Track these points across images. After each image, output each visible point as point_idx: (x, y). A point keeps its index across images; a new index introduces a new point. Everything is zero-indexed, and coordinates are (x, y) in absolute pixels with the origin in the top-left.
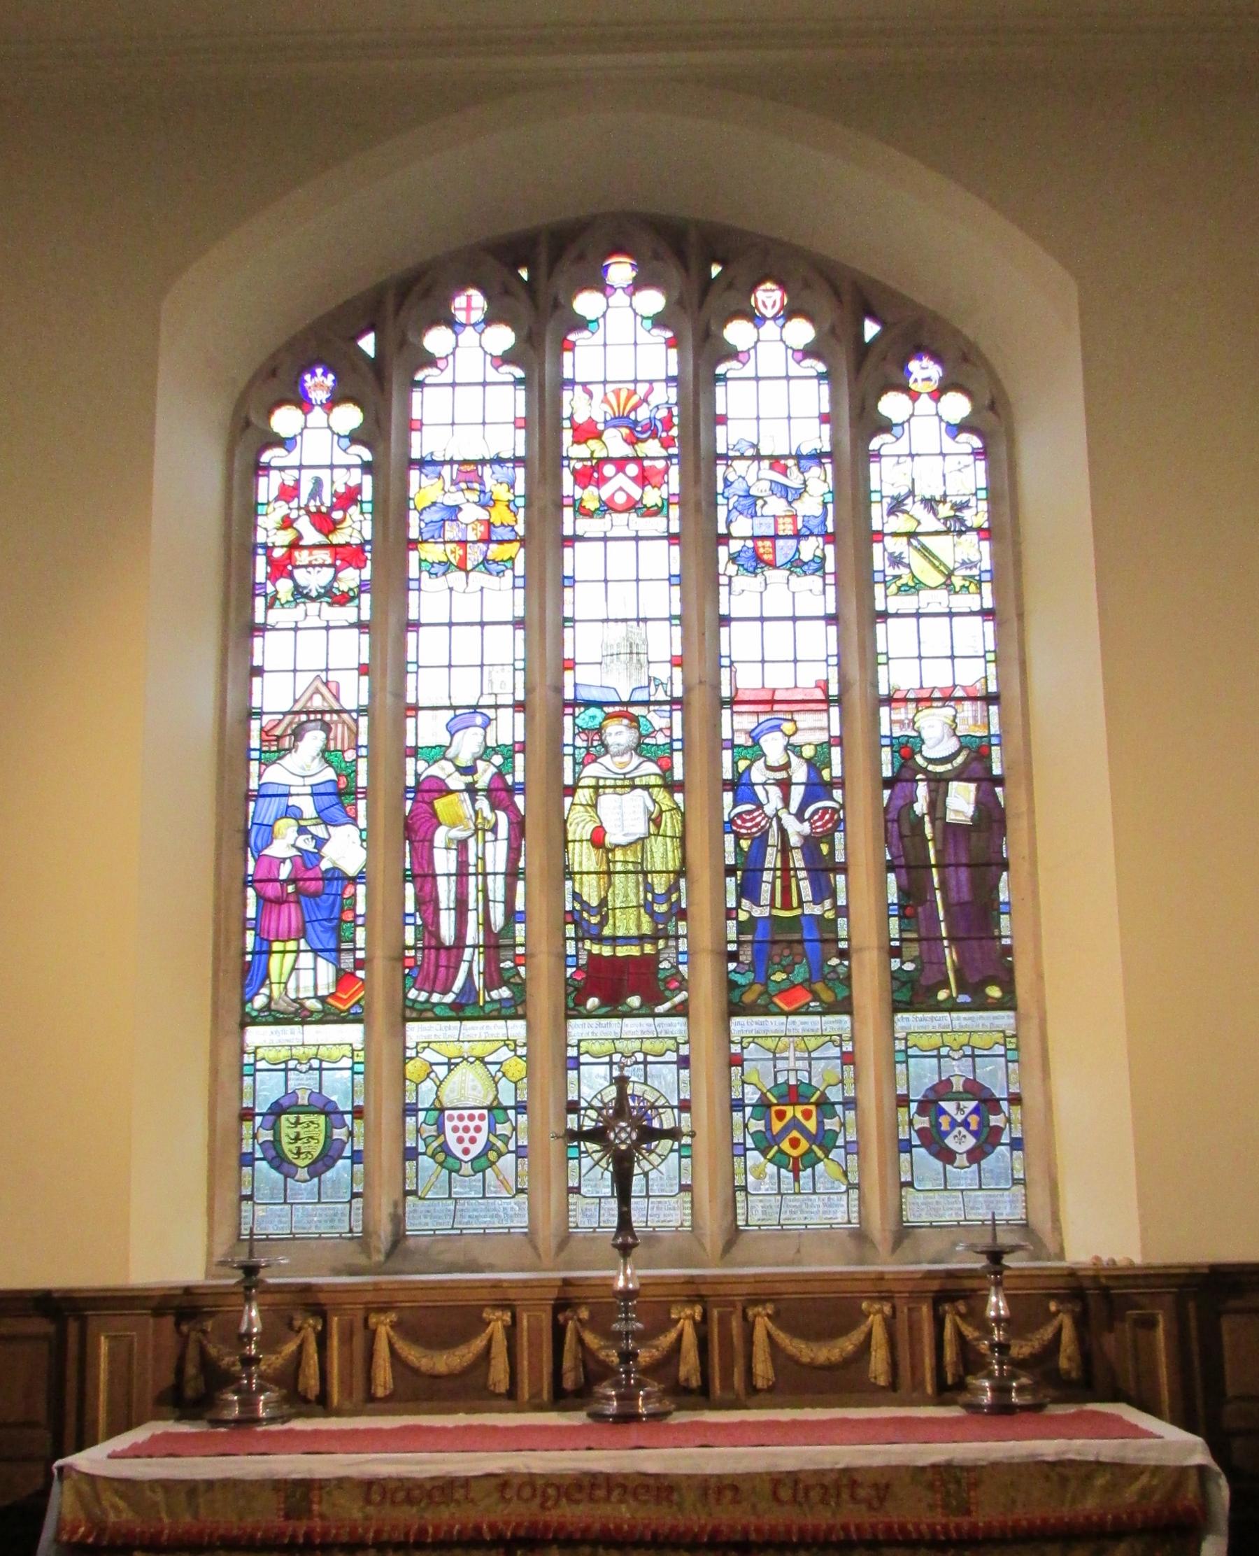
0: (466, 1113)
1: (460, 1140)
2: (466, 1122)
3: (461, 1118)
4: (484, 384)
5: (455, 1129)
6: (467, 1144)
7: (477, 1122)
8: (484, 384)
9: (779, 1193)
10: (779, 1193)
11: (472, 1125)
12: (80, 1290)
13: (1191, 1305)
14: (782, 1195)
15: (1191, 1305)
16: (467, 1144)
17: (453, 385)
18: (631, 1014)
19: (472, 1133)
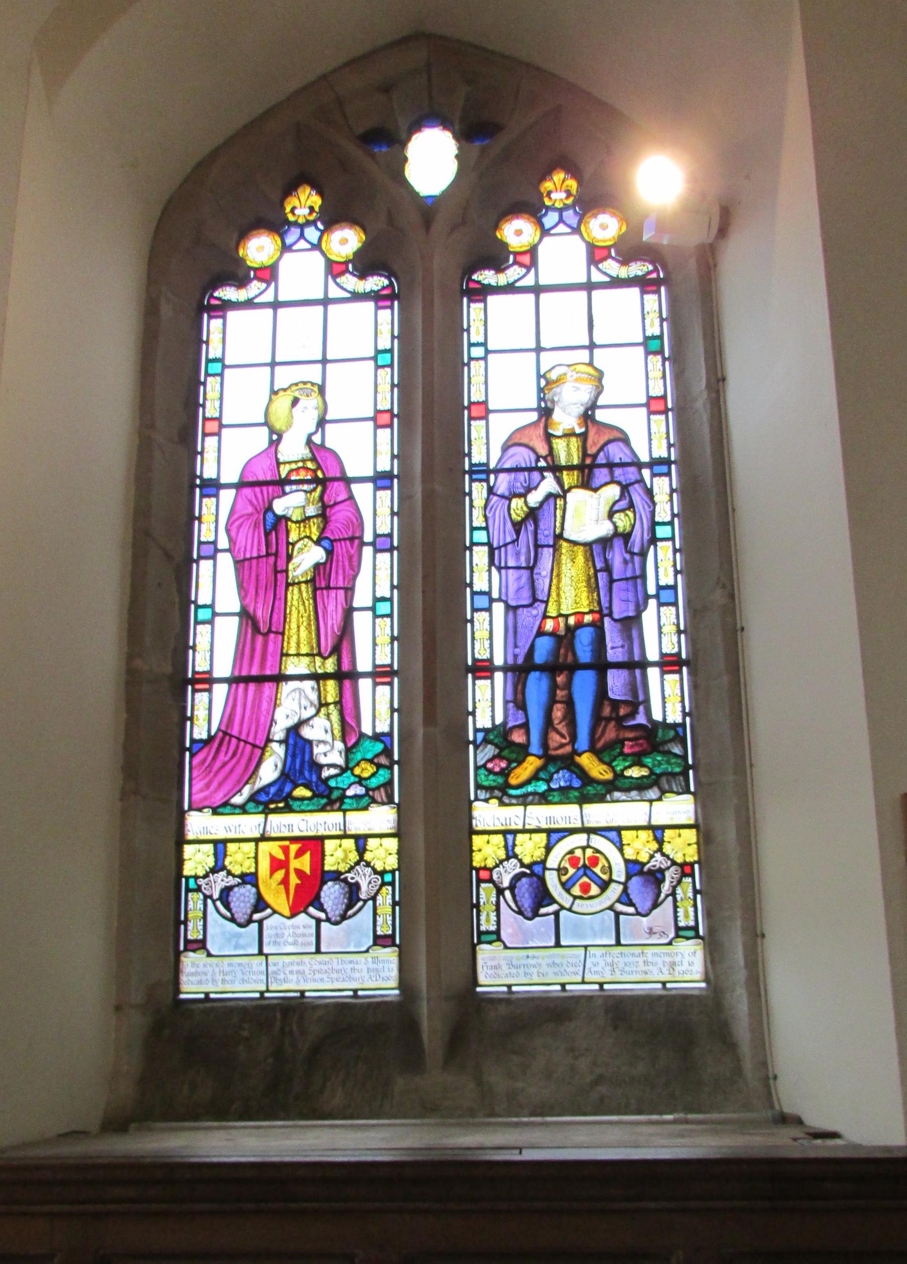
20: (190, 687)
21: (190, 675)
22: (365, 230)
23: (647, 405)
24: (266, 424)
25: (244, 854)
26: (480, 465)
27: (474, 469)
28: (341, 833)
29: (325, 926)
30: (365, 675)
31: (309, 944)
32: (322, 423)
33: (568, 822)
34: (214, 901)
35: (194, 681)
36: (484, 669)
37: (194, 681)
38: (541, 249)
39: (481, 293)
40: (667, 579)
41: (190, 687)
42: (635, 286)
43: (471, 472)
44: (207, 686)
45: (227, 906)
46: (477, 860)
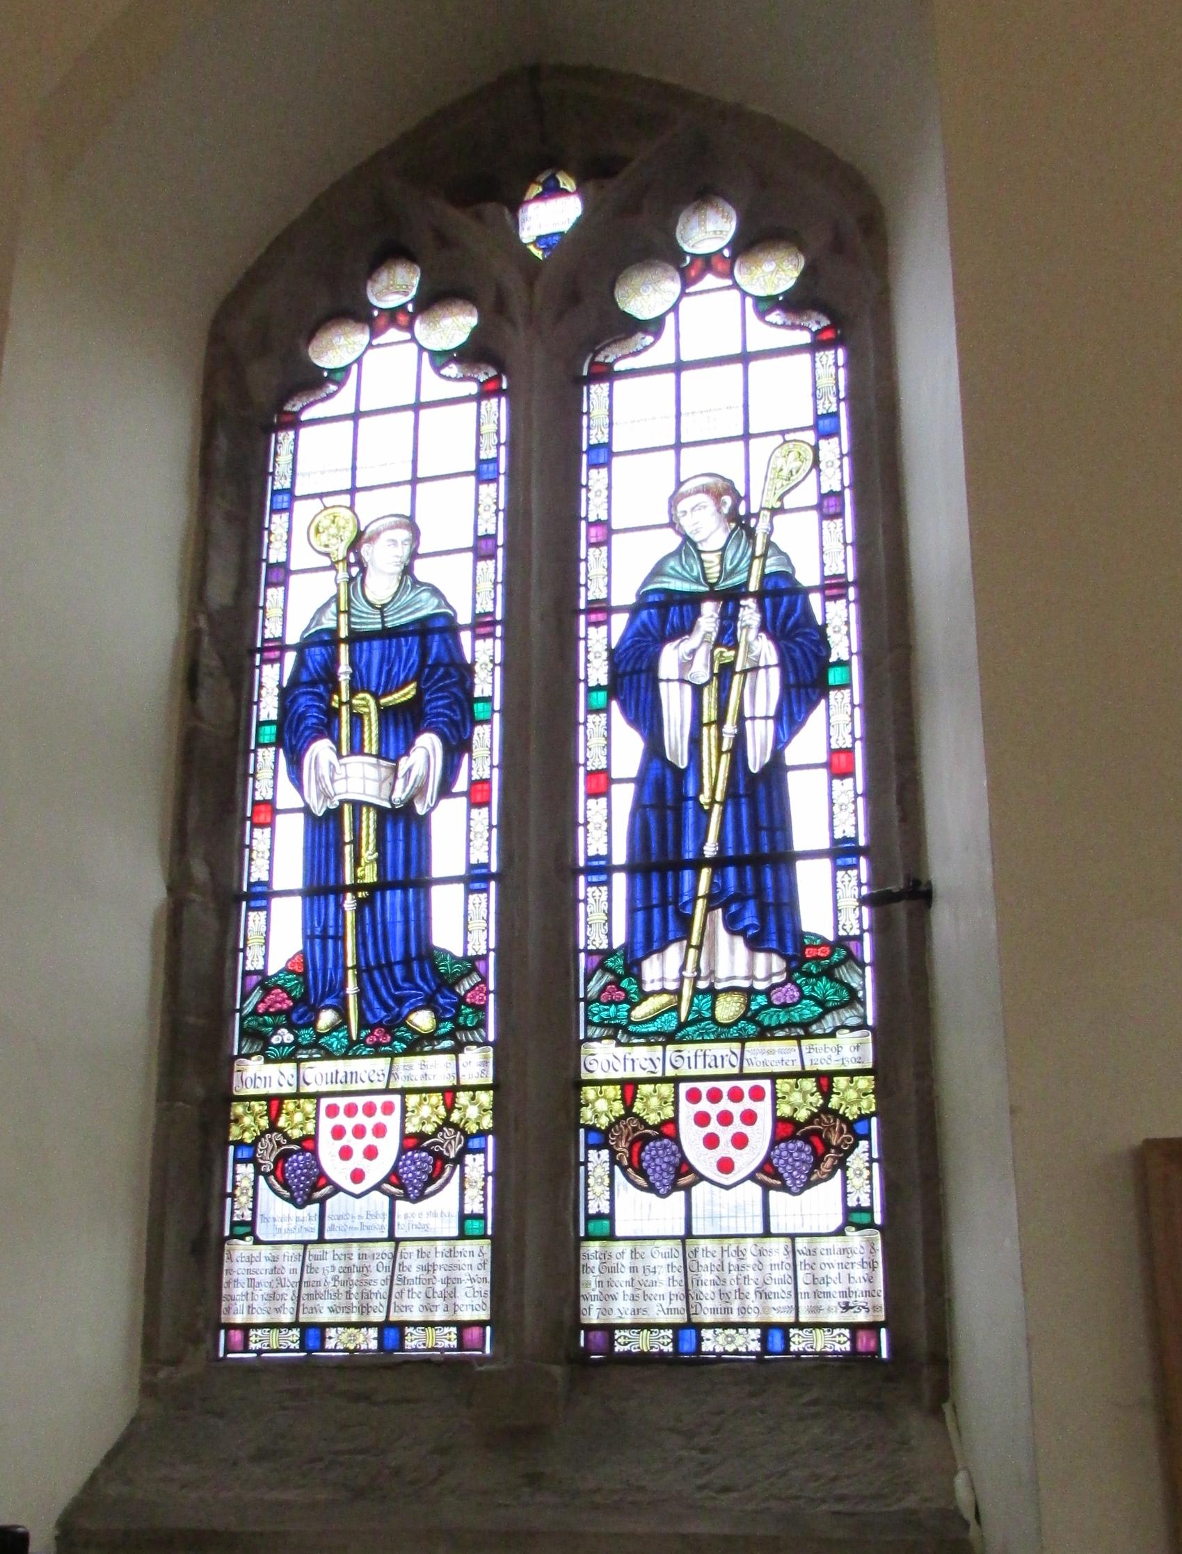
0: (360, 1101)
1: (346, 1153)
2: (725, 1104)
3: (351, 1111)
4: (745, 358)
5: (702, 1119)
6: (358, 1160)
7: (747, 1103)
8: (745, 358)
9: (391, 1237)
10: (391, 1237)
11: (736, 1109)
12: (926, 851)
13: (754, 1357)
14: (398, 1241)
15: (754, 1357)
16: (358, 1160)
17: (678, 367)
18: (418, 1044)
19: (737, 1126)
20: (244, 904)
21: (245, 889)
22: (802, 248)
23: (819, 507)
24: (672, 524)
25: (859, 1091)
26: (274, 640)
27: (266, 645)
28: (736, 1071)
29: (400, 1205)
30: (619, 869)
31: (312, 1231)
32: (414, 555)
33: (692, 1064)
34: (624, 1169)
35: (250, 896)
36: (601, 869)
37: (250, 896)
38: (365, 358)
39: (606, 374)
40: (482, 771)
41: (244, 904)
42: (738, 362)
43: (845, 585)
44: (603, 878)
45: (642, 1173)
46: (587, 1115)
